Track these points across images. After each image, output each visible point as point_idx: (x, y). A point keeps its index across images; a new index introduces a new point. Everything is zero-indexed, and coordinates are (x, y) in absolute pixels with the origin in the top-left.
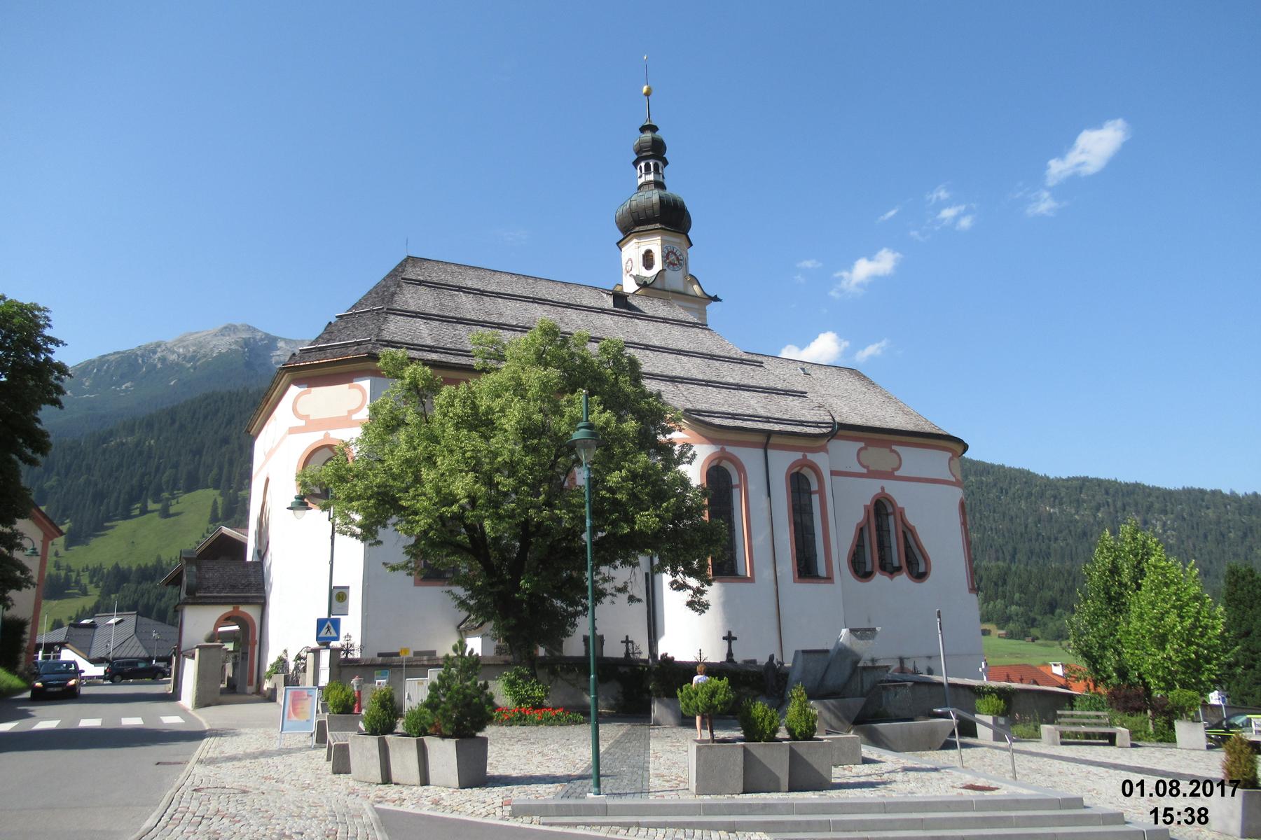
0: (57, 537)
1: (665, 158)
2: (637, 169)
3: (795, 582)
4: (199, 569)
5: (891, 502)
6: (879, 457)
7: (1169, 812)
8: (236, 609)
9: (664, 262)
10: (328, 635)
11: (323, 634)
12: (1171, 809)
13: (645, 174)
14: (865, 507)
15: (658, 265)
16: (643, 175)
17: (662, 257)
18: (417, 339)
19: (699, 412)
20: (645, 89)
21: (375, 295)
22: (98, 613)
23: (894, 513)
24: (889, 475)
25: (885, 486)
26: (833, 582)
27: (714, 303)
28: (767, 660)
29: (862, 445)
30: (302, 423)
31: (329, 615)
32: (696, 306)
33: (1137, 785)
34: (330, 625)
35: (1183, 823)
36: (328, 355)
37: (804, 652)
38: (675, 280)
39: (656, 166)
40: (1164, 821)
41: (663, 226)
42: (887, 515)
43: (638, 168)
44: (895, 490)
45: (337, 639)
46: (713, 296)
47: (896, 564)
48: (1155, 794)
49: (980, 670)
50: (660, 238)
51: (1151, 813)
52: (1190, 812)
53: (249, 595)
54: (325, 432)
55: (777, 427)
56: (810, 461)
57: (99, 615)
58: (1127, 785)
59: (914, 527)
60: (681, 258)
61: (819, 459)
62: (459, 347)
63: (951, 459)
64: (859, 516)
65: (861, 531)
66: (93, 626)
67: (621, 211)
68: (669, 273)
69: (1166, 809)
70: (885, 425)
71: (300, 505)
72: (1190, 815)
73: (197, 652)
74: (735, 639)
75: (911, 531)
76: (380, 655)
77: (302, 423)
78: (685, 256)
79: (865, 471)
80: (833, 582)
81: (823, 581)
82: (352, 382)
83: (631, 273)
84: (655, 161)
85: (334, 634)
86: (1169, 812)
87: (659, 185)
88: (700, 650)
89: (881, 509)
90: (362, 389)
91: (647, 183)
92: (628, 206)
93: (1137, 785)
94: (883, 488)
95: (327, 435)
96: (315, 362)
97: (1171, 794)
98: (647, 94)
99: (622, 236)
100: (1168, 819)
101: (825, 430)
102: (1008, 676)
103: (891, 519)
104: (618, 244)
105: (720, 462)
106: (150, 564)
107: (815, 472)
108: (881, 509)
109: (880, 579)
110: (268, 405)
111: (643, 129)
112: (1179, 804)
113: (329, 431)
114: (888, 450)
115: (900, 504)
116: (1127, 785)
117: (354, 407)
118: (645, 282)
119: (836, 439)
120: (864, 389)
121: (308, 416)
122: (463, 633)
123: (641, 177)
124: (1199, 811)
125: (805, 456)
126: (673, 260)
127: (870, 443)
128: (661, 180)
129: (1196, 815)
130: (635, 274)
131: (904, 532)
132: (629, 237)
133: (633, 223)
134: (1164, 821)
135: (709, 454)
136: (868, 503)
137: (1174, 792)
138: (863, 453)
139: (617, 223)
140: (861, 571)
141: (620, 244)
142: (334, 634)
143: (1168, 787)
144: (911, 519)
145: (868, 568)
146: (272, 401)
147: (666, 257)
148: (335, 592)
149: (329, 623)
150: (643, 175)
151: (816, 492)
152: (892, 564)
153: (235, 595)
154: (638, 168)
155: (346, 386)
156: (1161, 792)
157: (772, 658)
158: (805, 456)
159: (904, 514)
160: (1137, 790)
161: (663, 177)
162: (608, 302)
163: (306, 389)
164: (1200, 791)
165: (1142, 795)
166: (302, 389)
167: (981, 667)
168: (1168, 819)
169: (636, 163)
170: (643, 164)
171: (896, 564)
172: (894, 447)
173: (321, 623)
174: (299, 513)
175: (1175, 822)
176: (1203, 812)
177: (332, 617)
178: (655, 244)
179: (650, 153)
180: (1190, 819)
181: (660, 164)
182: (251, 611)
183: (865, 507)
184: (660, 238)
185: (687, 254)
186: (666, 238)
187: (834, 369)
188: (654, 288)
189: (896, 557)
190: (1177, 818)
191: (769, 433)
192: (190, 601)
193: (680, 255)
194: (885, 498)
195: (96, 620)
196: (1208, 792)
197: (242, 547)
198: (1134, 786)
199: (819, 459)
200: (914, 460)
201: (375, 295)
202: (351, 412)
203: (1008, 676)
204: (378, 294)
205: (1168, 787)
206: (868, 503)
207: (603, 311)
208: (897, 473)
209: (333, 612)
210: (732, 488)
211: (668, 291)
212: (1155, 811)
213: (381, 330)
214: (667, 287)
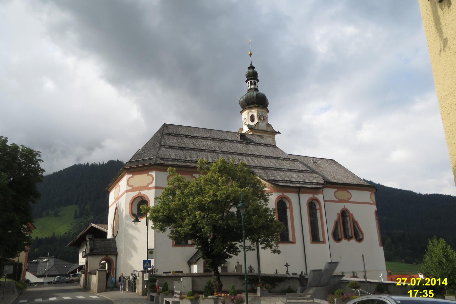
0: (33, 229)
1: (258, 79)
2: (247, 83)
3: (311, 243)
4: (93, 242)
5: (347, 211)
6: (343, 194)
10: (147, 266)
11: (145, 266)
13: (250, 85)
14: (338, 213)
16: (250, 86)
17: (258, 117)
18: (171, 157)
19: (274, 181)
20: (249, 53)
21: (154, 140)
22: (39, 257)
23: (349, 216)
24: (347, 201)
25: (345, 206)
26: (326, 244)
27: (278, 134)
28: (300, 273)
29: (336, 190)
30: (130, 188)
31: (147, 259)
32: (271, 136)
34: (148, 263)
36: (139, 163)
37: (313, 270)
38: (263, 126)
39: (254, 82)
41: (258, 105)
42: (347, 216)
44: (349, 207)
45: (150, 267)
46: (277, 131)
47: (350, 235)
49: (381, 276)
53: (111, 251)
55: (303, 186)
56: (315, 197)
57: (40, 258)
59: (357, 221)
60: (265, 117)
61: (320, 197)
62: (185, 159)
63: (371, 194)
64: (335, 217)
65: (336, 223)
66: (37, 263)
67: (241, 100)
68: (260, 123)
70: (345, 182)
71: (136, 220)
73: (97, 273)
74: (289, 265)
75: (356, 222)
76: (164, 273)
77: (130, 188)
78: (266, 116)
79: (337, 200)
80: (326, 244)
81: (321, 243)
83: (246, 124)
84: (254, 80)
85: (149, 266)
87: (256, 90)
88: (276, 270)
89: (344, 214)
90: (152, 176)
92: (244, 98)
94: (344, 206)
95: (140, 193)
96: (135, 166)
98: (251, 55)
99: (242, 109)
101: (321, 186)
102: (391, 278)
103: (348, 218)
104: (241, 112)
105: (282, 199)
106: (50, 236)
107: (318, 202)
108: (344, 214)
109: (344, 241)
110: (116, 181)
113: (140, 191)
114: (346, 191)
115: (351, 212)
117: (149, 182)
118: (252, 127)
119: (326, 188)
120: (337, 167)
121: (133, 186)
122: (190, 264)
123: (249, 86)
125: (314, 196)
127: (339, 189)
128: (257, 87)
130: (247, 124)
131: (353, 223)
132: (245, 110)
133: (246, 104)
135: (277, 197)
136: (339, 212)
138: (337, 193)
140: (337, 238)
141: (241, 112)
142: (149, 266)
144: (356, 218)
145: (340, 237)
146: (119, 179)
147: (259, 118)
148: (149, 251)
149: (147, 262)
150: (250, 86)
151: (318, 209)
152: (349, 235)
153: (106, 251)
154: (248, 82)
157: (302, 273)
158: (314, 196)
159: (353, 216)
161: (257, 86)
162: (239, 138)
167: (381, 275)
169: (247, 81)
170: (249, 81)
171: (350, 235)
172: (349, 190)
173: (145, 262)
174: (136, 223)
177: (148, 260)
178: (255, 112)
179: (252, 77)
181: (256, 81)
183: (338, 213)
184: (257, 110)
185: (267, 115)
187: (325, 160)
188: (255, 129)
189: (351, 232)
191: (300, 188)
193: (264, 116)
194: (345, 210)
195: (39, 260)
197: (106, 234)
199: (320, 197)
200: (356, 195)
201: (154, 140)
202: (148, 184)
203: (391, 278)
204: (155, 139)
206: (339, 212)
207: (236, 142)
208: (350, 200)
209: (149, 258)
210: (287, 208)
211: (260, 130)
213: (158, 154)
214: (260, 129)
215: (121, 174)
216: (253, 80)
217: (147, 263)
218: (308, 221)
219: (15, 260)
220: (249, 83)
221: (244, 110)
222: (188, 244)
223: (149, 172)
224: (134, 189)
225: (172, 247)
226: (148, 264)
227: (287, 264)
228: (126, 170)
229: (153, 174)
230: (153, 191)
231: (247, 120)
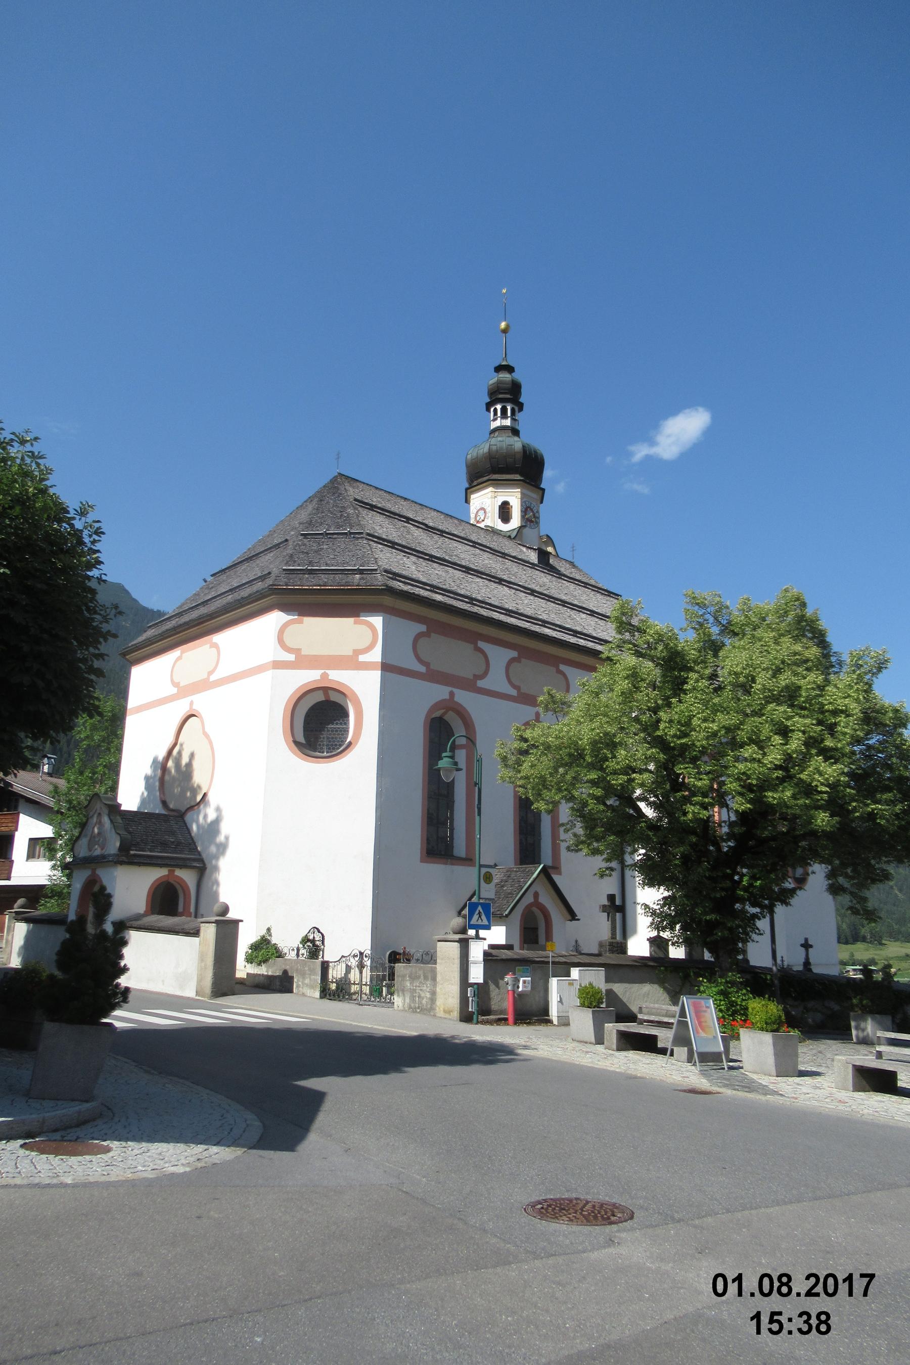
7: (776, 1317)
8: (171, 872)
9: (523, 517)
12: (780, 1313)
15: (516, 521)
16: (499, 419)
20: (503, 325)
30: (291, 657)
33: (734, 1281)
34: (481, 911)
35: (796, 1333)
40: (770, 1330)
43: (492, 409)
48: (757, 1293)
50: (519, 490)
51: (752, 1319)
52: (805, 1317)
54: (323, 671)
58: (720, 1281)
69: (773, 1314)
72: (805, 1322)
82: (358, 616)
86: (776, 1317)
87: (515, 432)
90: (372, 627)
91: (502, 428)
93: (734, 1281)
95: (324, 676)
97: (779, 1291)
98: (505, 331)
100: (775, 1327)
111: (499, 369)
112: (789, 1307)
113: (327, 671)
116: (720, 1281)
123: (495, 420)
124: (818, 1316)
126: (530, 517)
129: (814, 1322)
134: (770, 1330)
137: (785, 1290)
139: (467, 466)
143: (776, 1284)
149: (480, 908)
150: (499, 419)
154: (492, 409)
155: (351, 620)
156: (766, 1289)
160: (733, 1288)
162: (533, 557)
163: (296, 617)
164: (819, 1289)
165: (740, 1294)
166: (291, 617)
168: (775, 1327)
169: (488, 406)
175: (785, 1331)
176: (823, 1317)
178: (514, 497)
179: (508, 396)
180: (805, 1328)
181: (516, 409)
182: (187, 877)
186: (526, 492)
190: (787, 1326)
192: (124, 858)
196: (831, 1290)
198: (729, 1281)
202: (357, 652)
205: (776, 1284)
212: (757, 1316)
215: (244, 606)
216: (509, 404)
217: (480, 913)
218: (514, 821)
219: (607, 862)
220: (495, 410)
221: (481, 486)
222: (453, 856)
223: (361, 614)
224: (302, 661)
225: (421, 862)
226: (483, 917)
227: (806, 940)
228: (276, 594)
229: (377, 621)
230: (376, 676)
231: (489, 515)
